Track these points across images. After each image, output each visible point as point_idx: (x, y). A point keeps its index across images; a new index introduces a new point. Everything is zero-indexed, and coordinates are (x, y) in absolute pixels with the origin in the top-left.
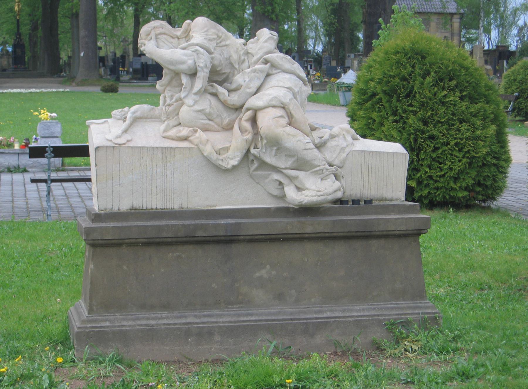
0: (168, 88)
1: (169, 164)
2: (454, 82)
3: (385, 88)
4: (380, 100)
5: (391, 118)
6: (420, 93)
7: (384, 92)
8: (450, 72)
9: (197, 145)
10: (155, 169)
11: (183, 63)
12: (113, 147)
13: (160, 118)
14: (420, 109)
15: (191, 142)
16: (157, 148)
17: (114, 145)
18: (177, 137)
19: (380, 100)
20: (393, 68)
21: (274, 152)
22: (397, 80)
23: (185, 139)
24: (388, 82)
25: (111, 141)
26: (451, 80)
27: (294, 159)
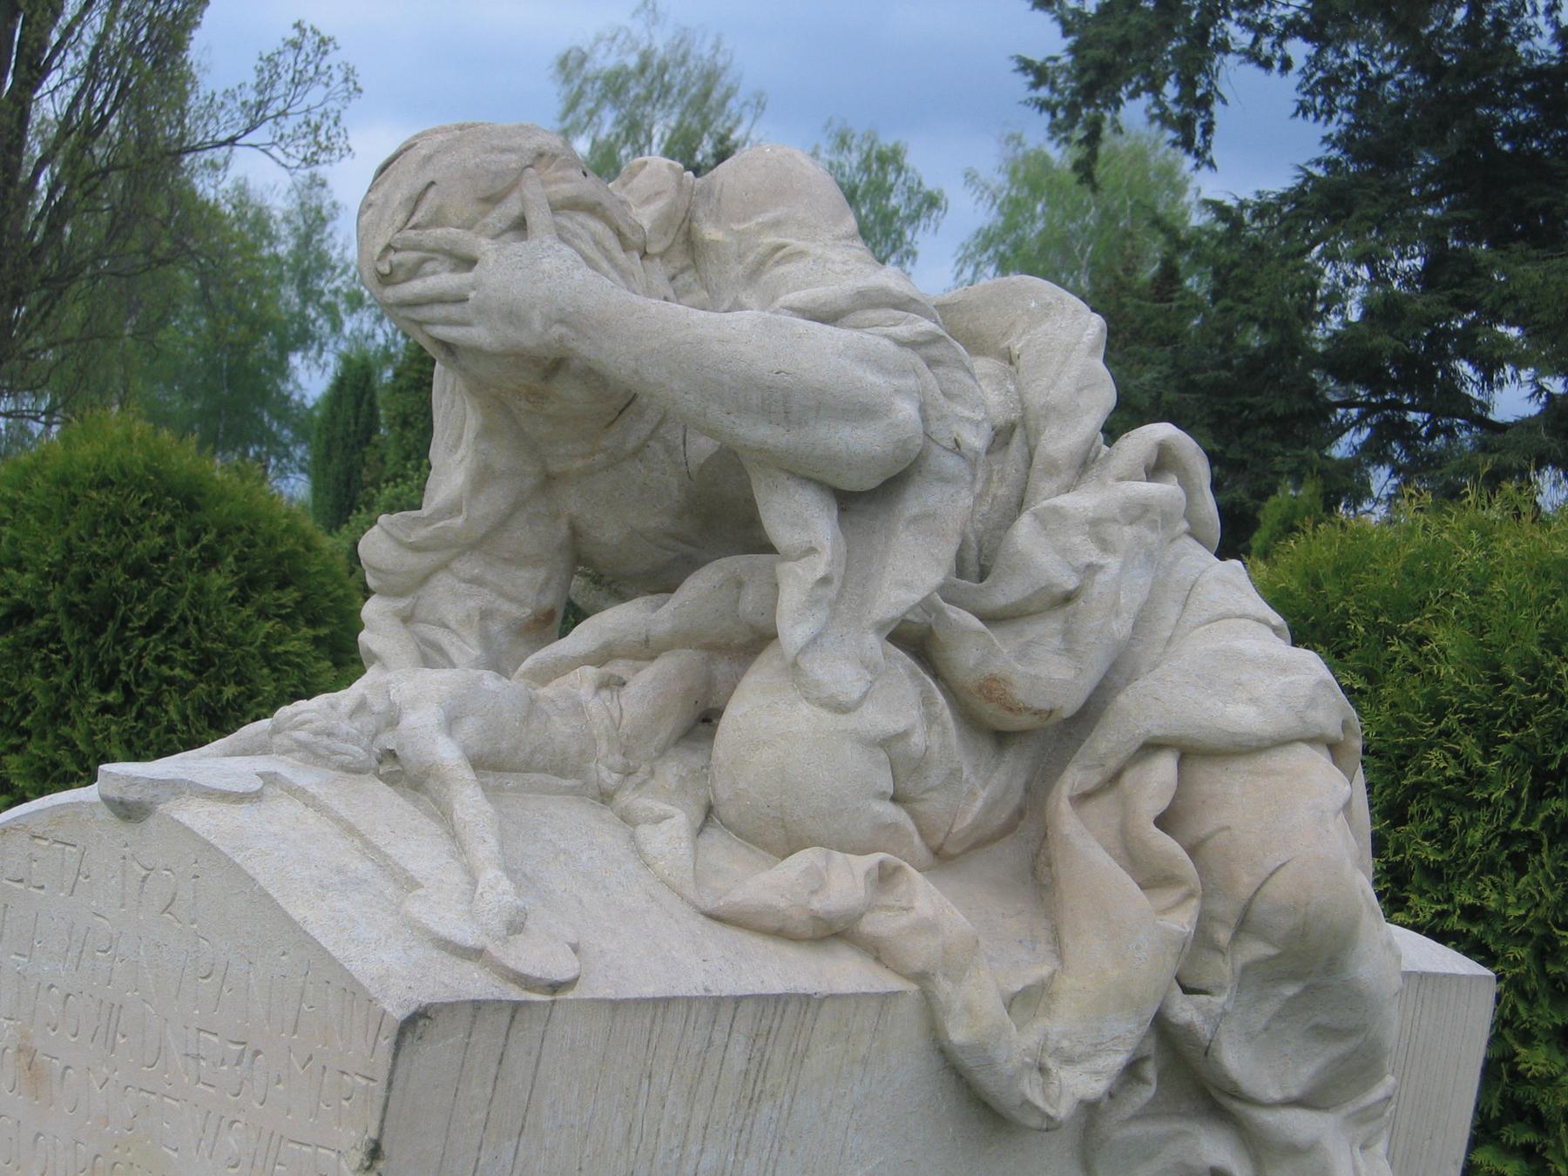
0: (468, 566)
1: (766, 1108)
2: (290, 596)
3: (76, 598)
4: (54, 633)
5: (96, 697)
6: (197, 621)
7: (71, 609)
8: (280, 559)
9: (921, 977)
10: (694, 1149)
11: (863, 410)
12: (517, 1007)
13: (578, 772)
14: (198, 673)
15: (875, 951)
16: (738, 1000)
17: (516, 994)
18: (816, 918)
19: (54, 633)
20: (101, 531)
21: (1271, 1007)
22: (120, 577)
23: (833, 933)
24: (85, 582)
25: (475, 954)
26: (283, 585)
27: (1338, 1049)
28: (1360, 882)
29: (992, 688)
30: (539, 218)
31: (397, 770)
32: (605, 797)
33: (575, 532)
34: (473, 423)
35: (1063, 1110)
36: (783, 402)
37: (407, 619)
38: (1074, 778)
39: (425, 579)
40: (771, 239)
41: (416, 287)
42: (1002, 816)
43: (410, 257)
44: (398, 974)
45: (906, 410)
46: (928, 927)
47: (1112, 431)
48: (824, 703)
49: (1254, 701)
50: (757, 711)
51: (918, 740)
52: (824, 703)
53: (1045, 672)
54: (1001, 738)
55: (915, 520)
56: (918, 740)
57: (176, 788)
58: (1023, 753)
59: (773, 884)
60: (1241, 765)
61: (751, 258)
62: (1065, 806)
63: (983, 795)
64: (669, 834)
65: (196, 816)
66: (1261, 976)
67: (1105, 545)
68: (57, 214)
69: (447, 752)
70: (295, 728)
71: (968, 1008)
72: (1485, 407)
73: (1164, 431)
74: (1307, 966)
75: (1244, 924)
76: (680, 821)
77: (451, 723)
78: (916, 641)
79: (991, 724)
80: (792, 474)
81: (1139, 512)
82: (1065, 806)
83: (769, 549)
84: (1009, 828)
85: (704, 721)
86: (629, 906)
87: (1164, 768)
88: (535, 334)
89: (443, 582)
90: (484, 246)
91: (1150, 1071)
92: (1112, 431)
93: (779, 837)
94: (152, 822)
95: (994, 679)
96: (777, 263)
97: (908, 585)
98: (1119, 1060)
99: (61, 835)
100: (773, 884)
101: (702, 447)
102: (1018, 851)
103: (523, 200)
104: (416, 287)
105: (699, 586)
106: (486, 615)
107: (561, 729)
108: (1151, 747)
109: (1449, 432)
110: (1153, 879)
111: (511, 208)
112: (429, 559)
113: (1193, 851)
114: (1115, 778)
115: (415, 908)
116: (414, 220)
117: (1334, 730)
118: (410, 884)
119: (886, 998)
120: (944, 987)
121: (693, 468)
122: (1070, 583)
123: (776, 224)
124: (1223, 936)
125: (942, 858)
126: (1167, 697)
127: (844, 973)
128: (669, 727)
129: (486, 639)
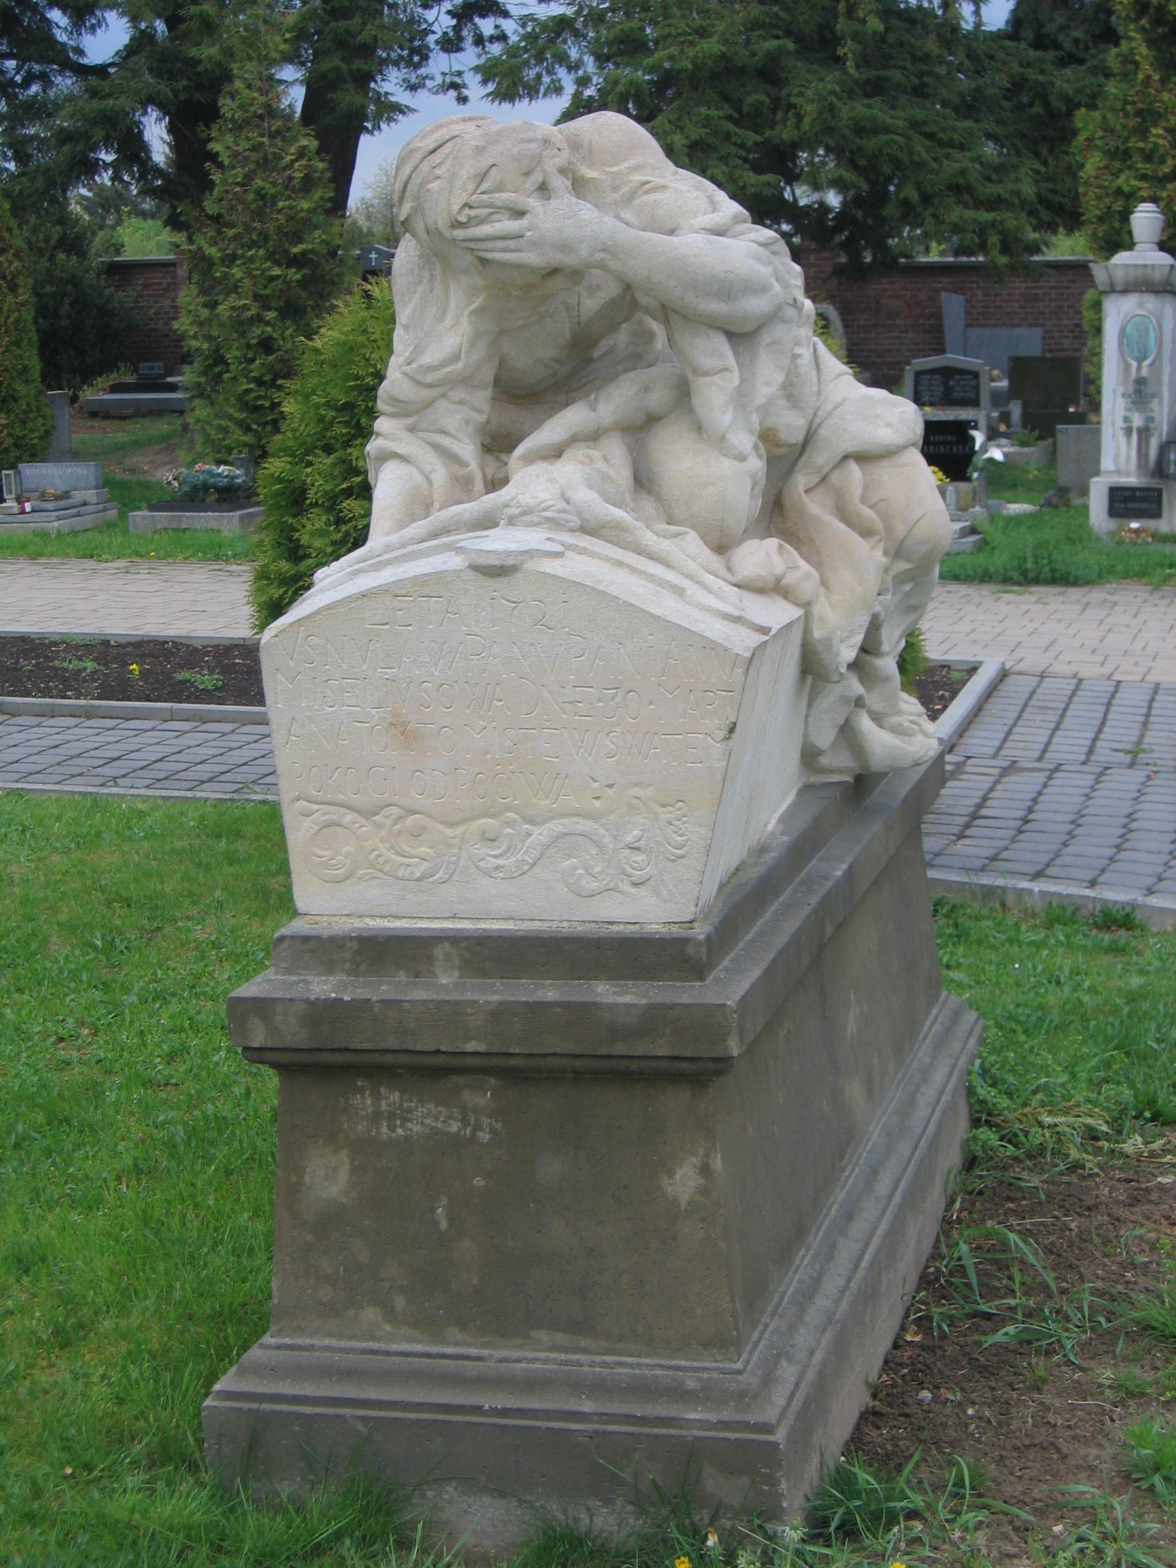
0: (458, 394)
39: (428, 404)
40: (637, 178)
41: (486, 230)
43: (484, 212)
49: (888, 425)
55: (768, 345)
60: (885, 463)
61: (625, 189)
62: (805, 497)
70: (545, 510)
71: (821, 619)
72: (80, 52)
80: (710, 326)
82: (805, 497)
89: (442, 405)
94: (519, 576)
95: (770, 429)
96: (646, 193)
97: (768, 384)
99: (426, 592)
103: (544, 172)
109: (44, 78)
111: (537, 177)
112: (435, 392)
116: (483, 188)
121: (582, 318)
123: (638, 168)
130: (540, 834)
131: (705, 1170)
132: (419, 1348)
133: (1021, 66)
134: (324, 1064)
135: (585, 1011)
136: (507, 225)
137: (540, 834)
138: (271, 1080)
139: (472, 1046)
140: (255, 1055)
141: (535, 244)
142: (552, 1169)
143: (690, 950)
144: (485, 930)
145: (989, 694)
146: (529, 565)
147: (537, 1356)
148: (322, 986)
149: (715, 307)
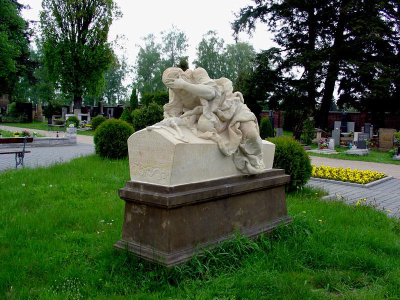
11: (210, 93)
23: (209, 139)
25: (181, 140)
28: (258, 134)
29: (223, 117)
30: (180, 76)
31: (173, 127)
32: (189, 128)
33: (183, 104)
34: (174, 95)
35: (230, 155)
36: (203, 92)
37: (168, 113)
38: (230, 125)
39: (170, 110)
41: (169, 83)
42: (224, 129)
44: (176, 142)
45: (214, 93)
46: (217, 138)
47: (233, 92)
48: (208, 119)
50: (202, 120)
51: (216, 122)
52: (208, 119)
53: (227, 116)
54: (224, 122)
56: (216, 122)
57: (154, 128)
58: (226, 124)
59: (203, 135)
63: (222, 127)
64: (195, 130)
65: (156, 131)
66: (248, 142)
67: (232, 103)
68: (109, 102)
69: (175, 124)
73: (238, 92)
74: (252, 141)
75: (247, 138)
76: (196, 130)
77: (175, 122)
78: (216, 113)
79: (222, 120)
81: (236, 100)
83: (202, 105)
84: (225, 130)
85: (197, 121)
86: (193, 138)
87: (239, 124)
88: (181, 87)
89: (171, 110)
90: (175, 79)
91: (239, 151)
92: (233, 92)
93: (204, 131)
98: (235, 150)
100: (203, 135)
101: (195, 96)
102: (225, 131)
104: (169, 83)
105: (195, 109)
106: (176, 113)
107: (185, 122)
108: (237, 122)
110: (238, 133)
111: (177, 76)
113: (242, 131)
114: (234, 125)
115: (175, 136)
117: (254, 119)
118: (174, 135)
119: (214, 144)
120: (219, 143)
122: (229, 107)
123: (201, 76)
124: (245, 139)
125: (219, 133)
126: (240, 117)
127: (210, 142)
128: (194, 122)
129: (176, 115)
130: (154, 170)
131: (167, 224)
132: (135, 244)
133: (46, 82)
134: (130, 201)
135: (152, 196)
136: (172, 82)
137: (154, 170)
138: (123, 202)
139: (141, 200)
140: (121, 198)
141: (175, 86)
142: (151, 220)
143: (167, 189)
144: (12, 147)
145: (387, 180)
146: (153, 130)
147: (146, 248)
148: (129, 189)
149: (203, 96)
